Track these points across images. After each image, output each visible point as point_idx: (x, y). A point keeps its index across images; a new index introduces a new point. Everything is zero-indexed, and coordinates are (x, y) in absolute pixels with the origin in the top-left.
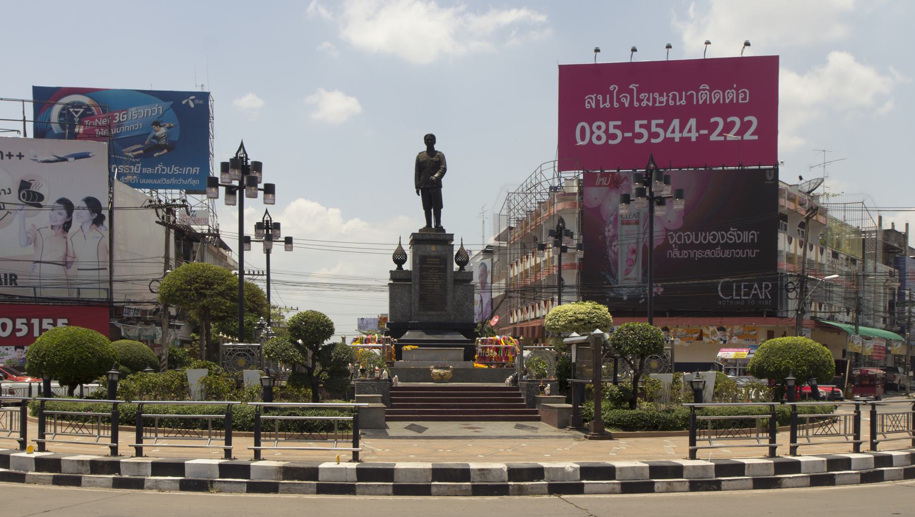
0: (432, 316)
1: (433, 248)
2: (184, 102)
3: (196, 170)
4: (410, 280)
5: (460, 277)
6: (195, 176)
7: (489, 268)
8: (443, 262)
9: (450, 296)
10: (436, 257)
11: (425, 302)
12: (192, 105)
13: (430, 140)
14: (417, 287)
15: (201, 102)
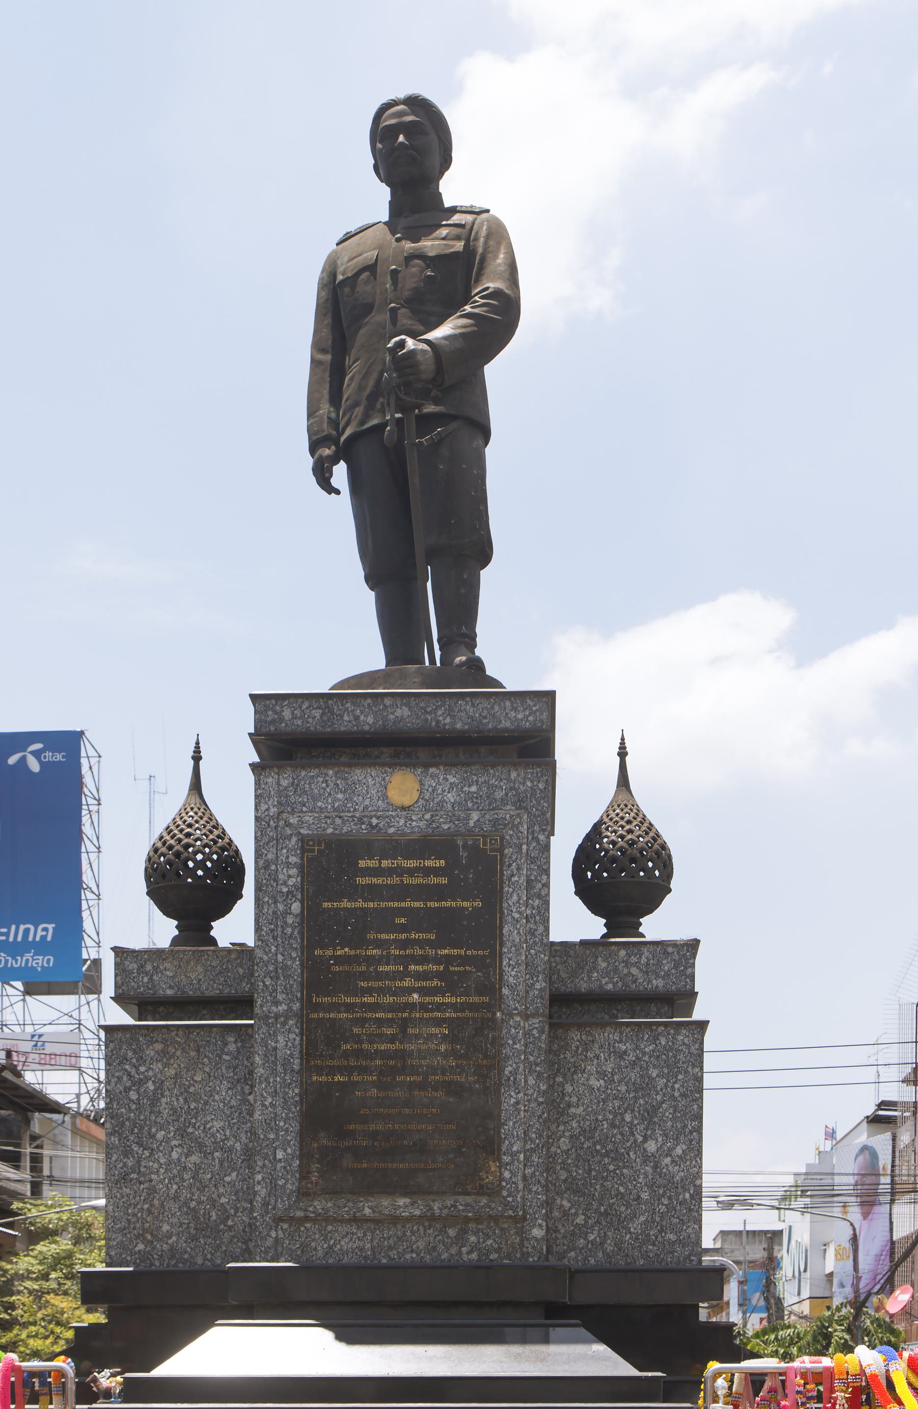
0: (399, 1228)
1: (403, 787)
2: (12, 760)
3: (45, 931)
4: (242, 1004)
5: (600, 978)
6: (41, 947)
7: (885, 1160)
8: (475, 881)
9: (520, 1100)
10: (423, 846)
11: (344, 1137)
12: (34, 765)
13: (411, 144)
14: (287, 1042)
15: (59, 757)
